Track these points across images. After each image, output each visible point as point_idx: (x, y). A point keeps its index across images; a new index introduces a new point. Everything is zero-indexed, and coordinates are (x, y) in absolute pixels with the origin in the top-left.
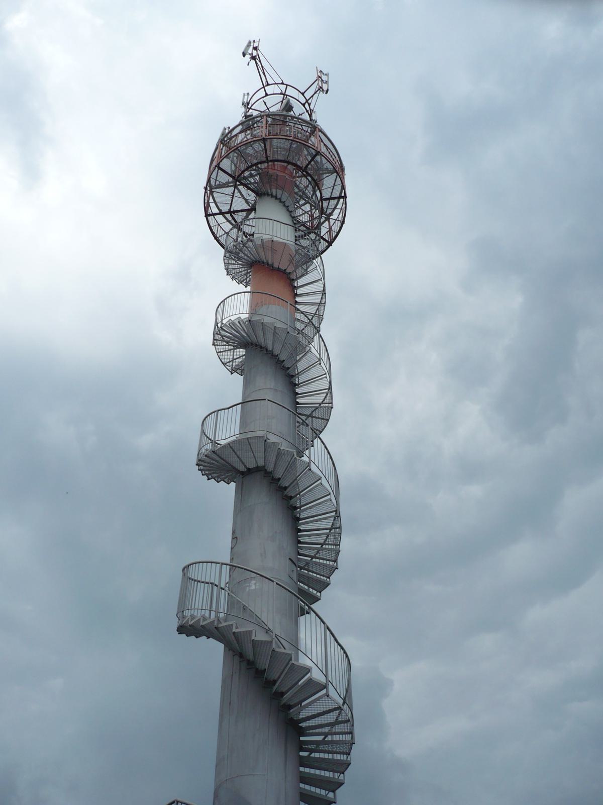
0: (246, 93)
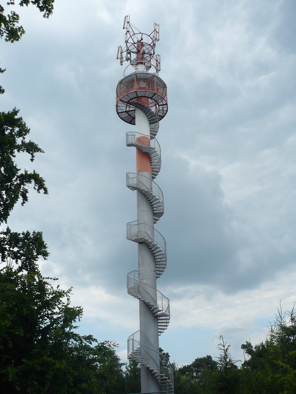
0: (126, 16)
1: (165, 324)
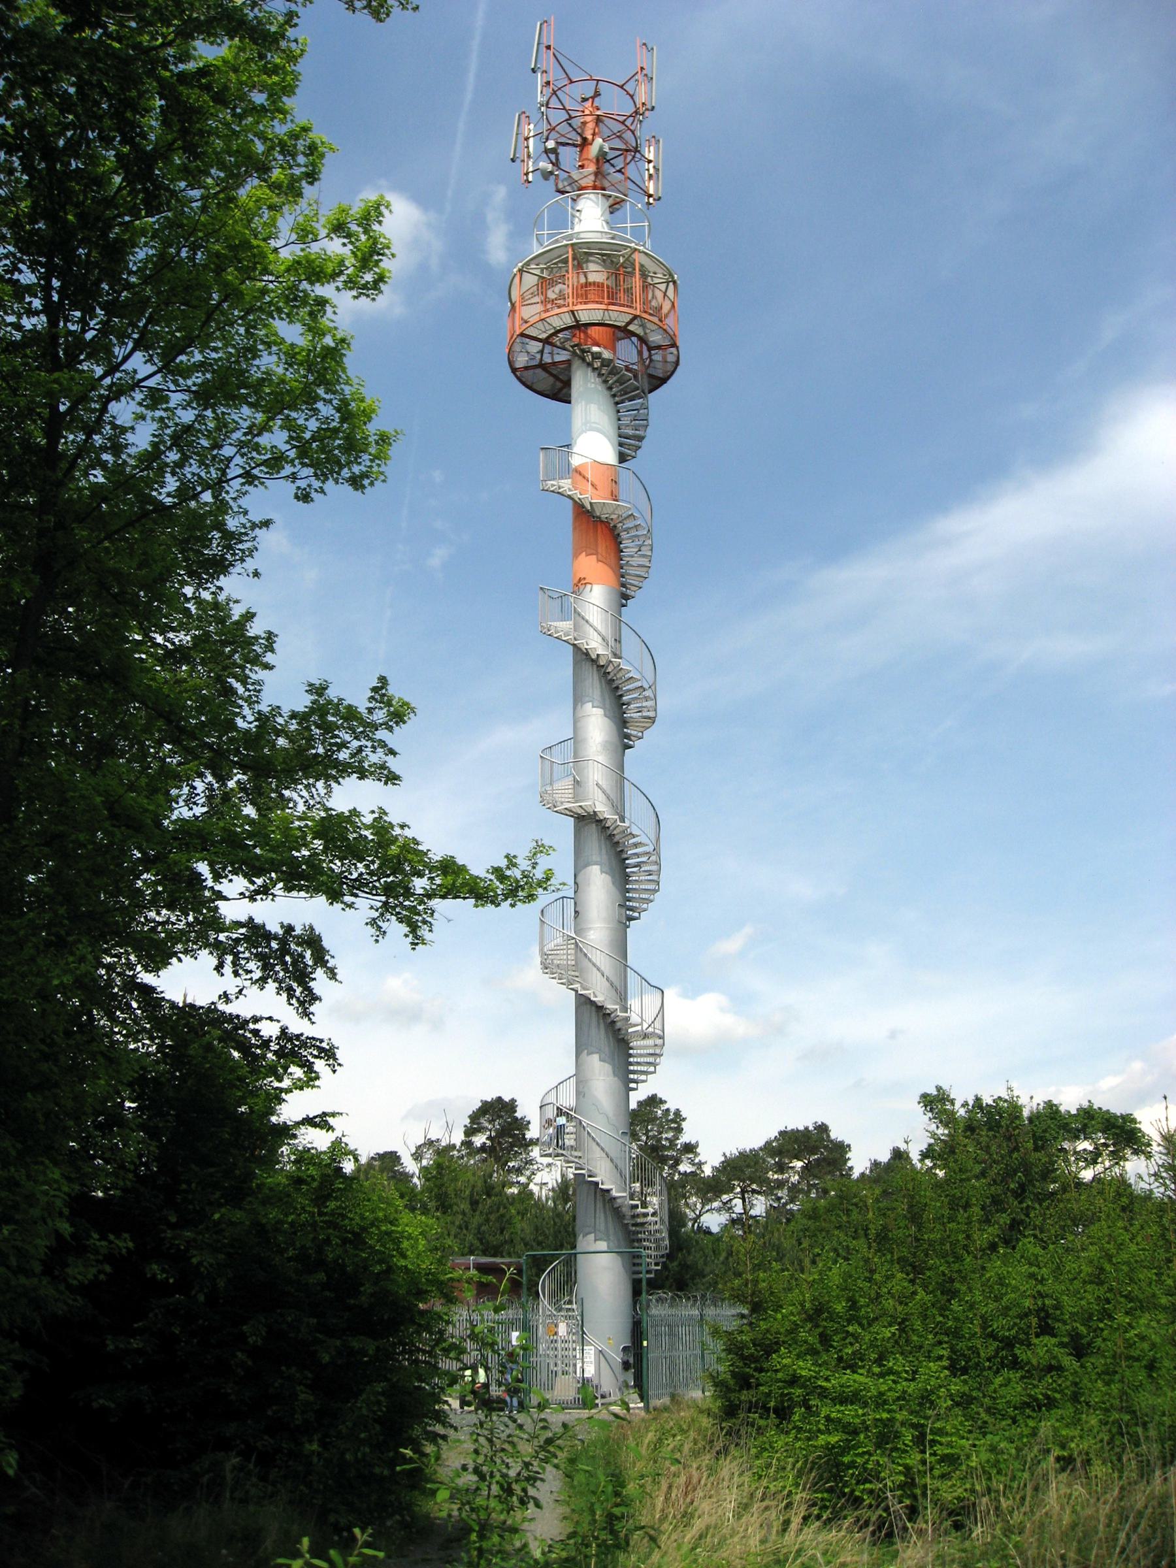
1: (651, 1059)
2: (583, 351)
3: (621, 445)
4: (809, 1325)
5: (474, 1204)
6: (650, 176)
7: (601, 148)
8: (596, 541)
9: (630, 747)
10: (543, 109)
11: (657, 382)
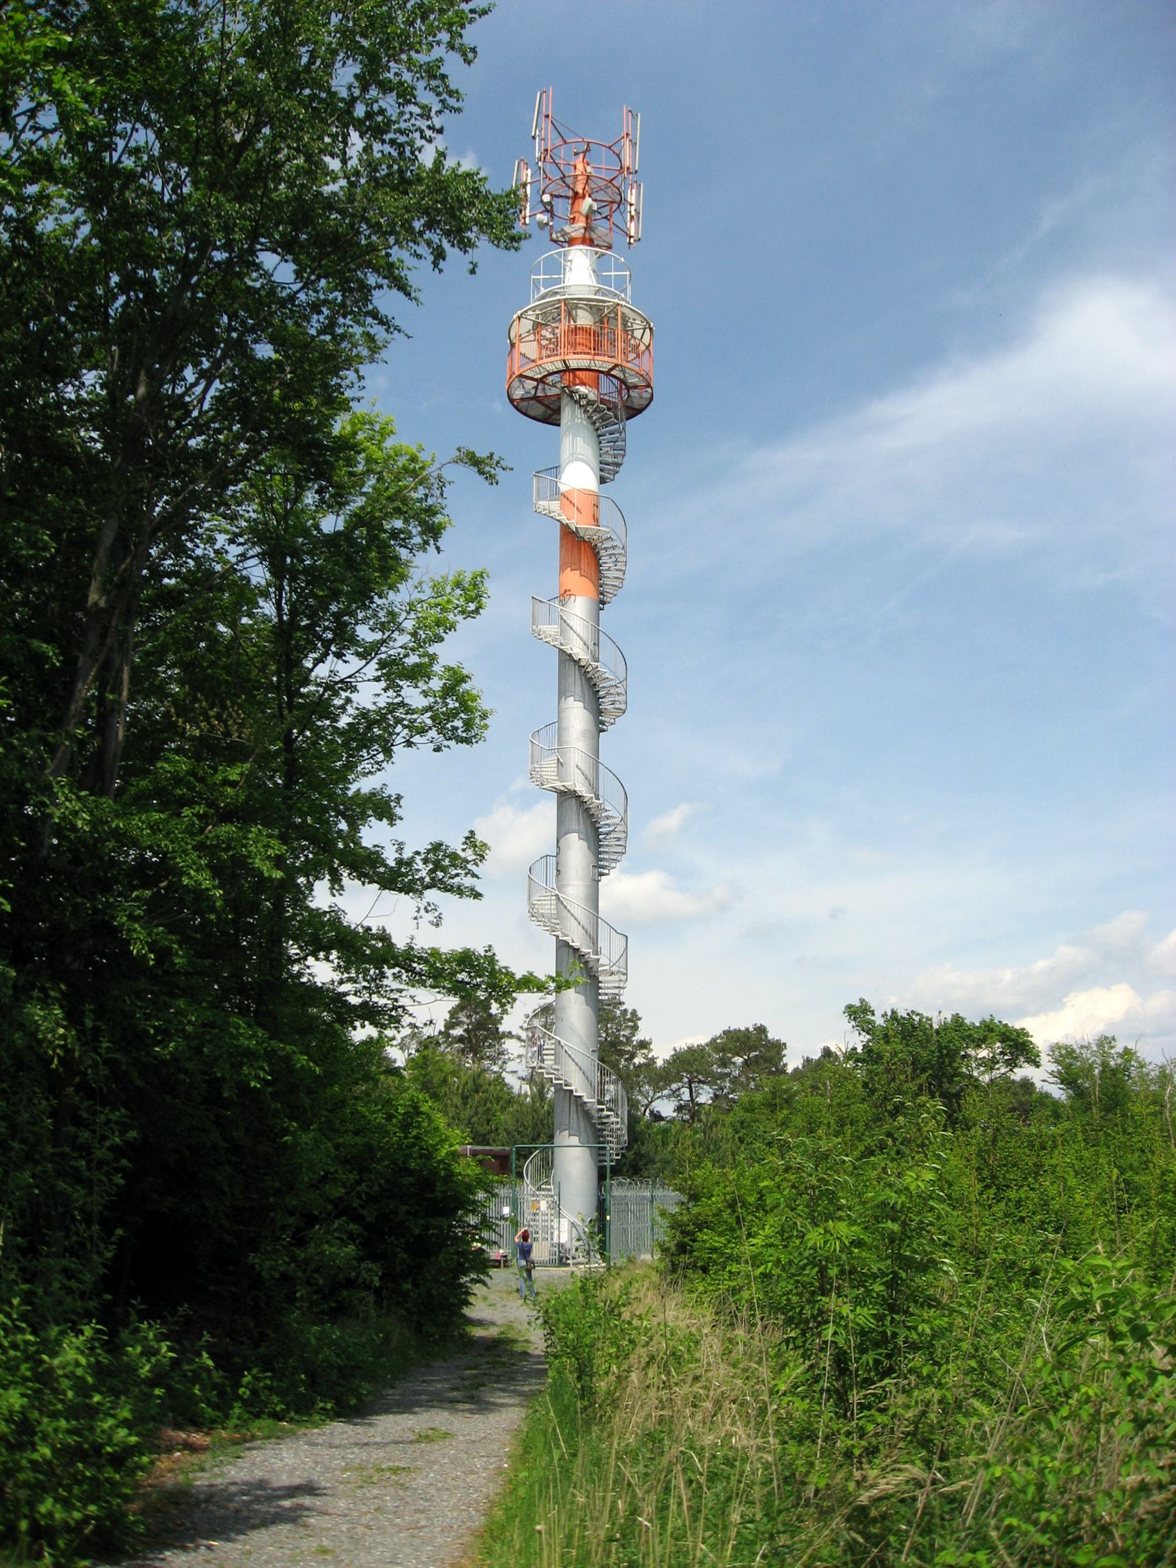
2: (572, 392)
3: (601, 470)
4: (729, 1211)
5: (465, 1098)
6: (632, 217)
7: (591, 207)
8: (580, 554)
9: (604, 731)
10: (540, 164)
11: (634, 412)
